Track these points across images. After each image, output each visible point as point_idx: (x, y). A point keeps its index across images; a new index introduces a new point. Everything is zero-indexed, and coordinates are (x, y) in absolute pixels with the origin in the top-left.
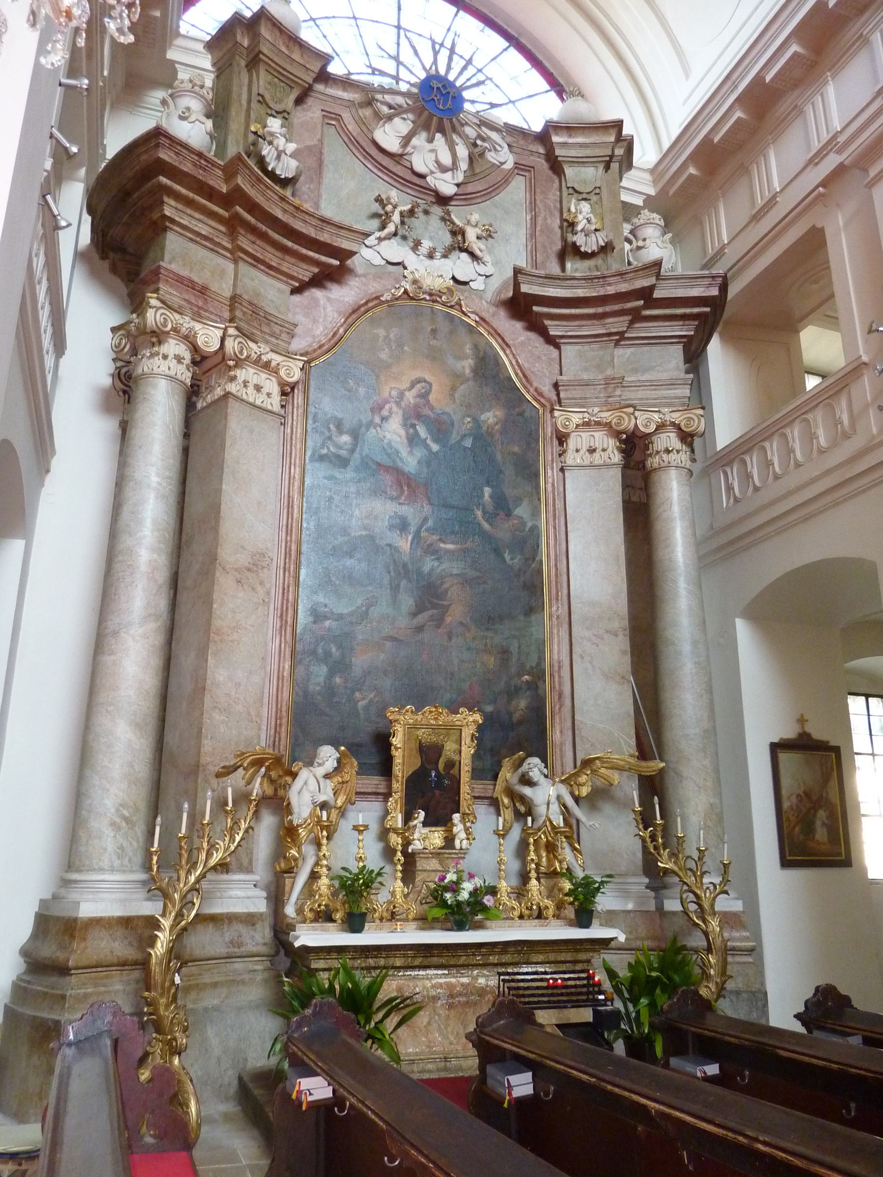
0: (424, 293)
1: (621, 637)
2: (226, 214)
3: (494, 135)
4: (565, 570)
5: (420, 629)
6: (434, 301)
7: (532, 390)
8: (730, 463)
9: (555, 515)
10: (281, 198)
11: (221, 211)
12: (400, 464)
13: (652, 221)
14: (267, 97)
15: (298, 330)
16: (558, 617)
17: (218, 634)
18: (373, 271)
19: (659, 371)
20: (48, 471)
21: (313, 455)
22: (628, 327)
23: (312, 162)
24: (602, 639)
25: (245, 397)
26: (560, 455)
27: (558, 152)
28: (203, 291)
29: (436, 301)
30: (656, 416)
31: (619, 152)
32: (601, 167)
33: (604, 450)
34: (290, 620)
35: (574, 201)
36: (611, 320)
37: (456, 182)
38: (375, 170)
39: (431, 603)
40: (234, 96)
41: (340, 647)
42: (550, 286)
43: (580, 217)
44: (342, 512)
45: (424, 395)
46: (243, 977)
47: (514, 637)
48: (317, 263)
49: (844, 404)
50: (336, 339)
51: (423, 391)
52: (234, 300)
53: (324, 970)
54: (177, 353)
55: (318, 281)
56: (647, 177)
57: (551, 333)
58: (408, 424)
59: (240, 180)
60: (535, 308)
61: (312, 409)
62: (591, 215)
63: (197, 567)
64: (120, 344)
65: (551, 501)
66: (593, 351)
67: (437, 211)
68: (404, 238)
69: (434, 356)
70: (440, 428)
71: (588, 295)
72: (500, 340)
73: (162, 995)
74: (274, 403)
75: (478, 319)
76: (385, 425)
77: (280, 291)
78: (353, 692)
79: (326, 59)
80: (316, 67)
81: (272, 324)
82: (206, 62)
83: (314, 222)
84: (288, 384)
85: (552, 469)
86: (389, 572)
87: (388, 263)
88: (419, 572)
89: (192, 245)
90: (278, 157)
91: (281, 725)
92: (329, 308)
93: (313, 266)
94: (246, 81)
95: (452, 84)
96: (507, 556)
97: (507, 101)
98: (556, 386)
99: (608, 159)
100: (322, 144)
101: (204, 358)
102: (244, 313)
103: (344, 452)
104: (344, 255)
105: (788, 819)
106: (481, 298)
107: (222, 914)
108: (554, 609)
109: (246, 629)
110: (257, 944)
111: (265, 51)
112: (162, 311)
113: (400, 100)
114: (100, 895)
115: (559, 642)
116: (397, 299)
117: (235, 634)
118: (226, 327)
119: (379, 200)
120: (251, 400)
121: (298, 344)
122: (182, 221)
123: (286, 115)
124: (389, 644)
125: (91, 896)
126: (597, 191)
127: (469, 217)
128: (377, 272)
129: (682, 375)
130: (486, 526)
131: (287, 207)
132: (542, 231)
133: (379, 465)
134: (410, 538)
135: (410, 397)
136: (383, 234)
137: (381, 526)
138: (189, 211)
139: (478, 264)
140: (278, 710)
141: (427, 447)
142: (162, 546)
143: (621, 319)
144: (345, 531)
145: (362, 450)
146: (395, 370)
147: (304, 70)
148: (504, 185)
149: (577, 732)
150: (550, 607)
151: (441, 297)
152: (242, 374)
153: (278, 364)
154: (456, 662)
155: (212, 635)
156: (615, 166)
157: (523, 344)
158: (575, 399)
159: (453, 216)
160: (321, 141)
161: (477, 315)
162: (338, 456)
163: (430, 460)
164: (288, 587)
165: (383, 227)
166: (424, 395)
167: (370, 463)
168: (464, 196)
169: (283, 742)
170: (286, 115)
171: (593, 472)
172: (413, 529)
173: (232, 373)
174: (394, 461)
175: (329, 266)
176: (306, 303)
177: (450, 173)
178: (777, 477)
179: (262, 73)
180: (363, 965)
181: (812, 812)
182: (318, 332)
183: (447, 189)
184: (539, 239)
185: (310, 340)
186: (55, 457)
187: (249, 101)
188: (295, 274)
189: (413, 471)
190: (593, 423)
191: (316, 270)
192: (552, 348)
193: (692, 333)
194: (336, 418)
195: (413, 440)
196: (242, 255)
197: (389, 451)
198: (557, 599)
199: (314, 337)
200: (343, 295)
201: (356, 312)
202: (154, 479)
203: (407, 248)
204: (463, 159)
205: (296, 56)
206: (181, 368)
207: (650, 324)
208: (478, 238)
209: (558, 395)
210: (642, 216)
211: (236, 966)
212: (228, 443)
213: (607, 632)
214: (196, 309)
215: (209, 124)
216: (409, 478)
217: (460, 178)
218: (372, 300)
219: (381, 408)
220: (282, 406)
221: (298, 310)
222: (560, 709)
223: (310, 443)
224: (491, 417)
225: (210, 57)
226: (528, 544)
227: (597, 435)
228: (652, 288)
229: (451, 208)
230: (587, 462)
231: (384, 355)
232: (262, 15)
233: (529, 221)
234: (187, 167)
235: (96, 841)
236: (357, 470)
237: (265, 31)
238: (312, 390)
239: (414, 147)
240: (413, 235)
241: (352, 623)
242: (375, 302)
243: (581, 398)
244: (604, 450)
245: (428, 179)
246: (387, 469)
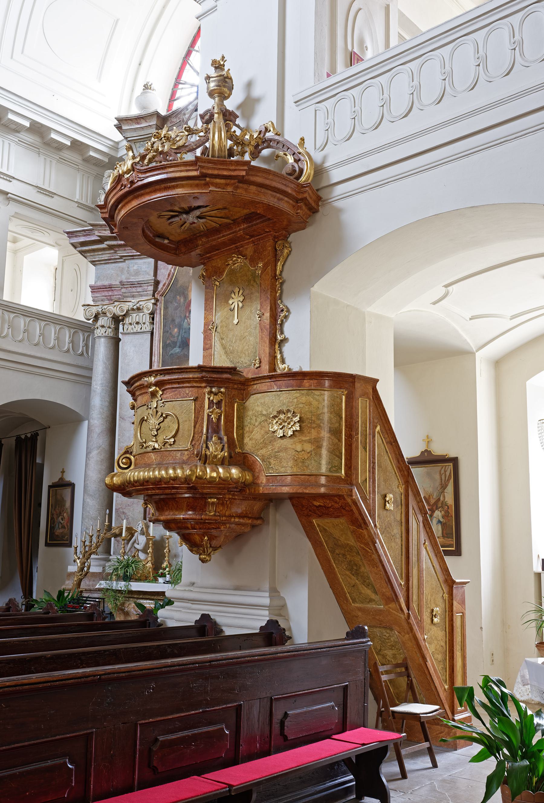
122: (96, 259)
236: (179, 347)
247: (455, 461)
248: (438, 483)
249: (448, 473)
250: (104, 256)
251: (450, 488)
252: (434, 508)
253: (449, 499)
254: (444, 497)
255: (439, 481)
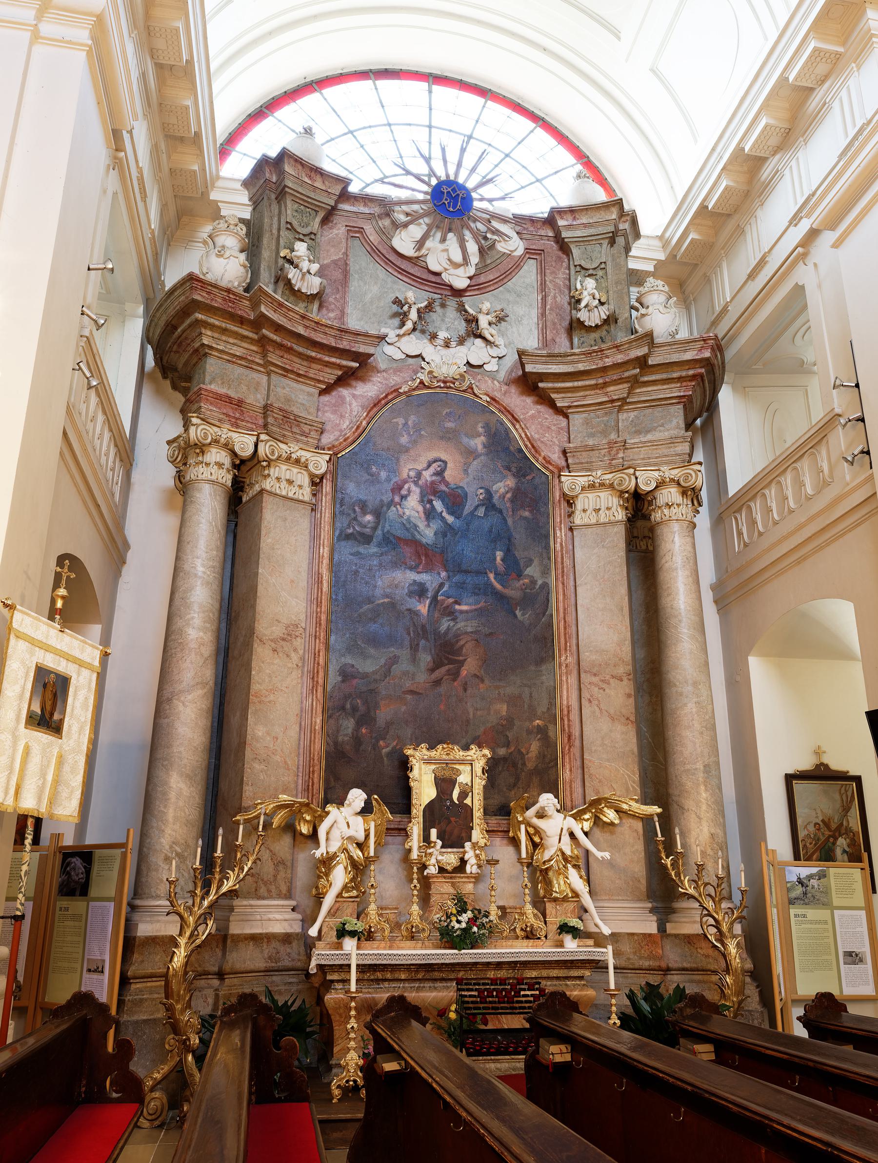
0: (438, 382)
1: (625, 682)
2: (255, 337)
3: (504, 228)
4: (574, 622)
5: (437, 683)
6: (448, 388)
7: (540, 459)
8: (739, 510)
9: (563, 572)
10: (301, 316)
11: (251, 335)
12: (418, 537)
13: (655, 288)
14: (295, 223)
15: (328, 427)
16: (567, 666)
17: (256, 697)
18: (395, 365)
19: (660, 431)
20: (124, 563)
21: (340, 535)
22: (629, 393)
23: (337, 274)
24: (609, 684)
25: (278, 492)
26: (569, 516)
27: (564, 234)
28: (239, 403)
29: (450, 387)
30: (656, 474)
31: (621, 226)
32: (605, 243)
33: (608, 509)
34: (321, 681)
35: (579, 278)
36: (612, 388)
37: (468, 275)
38: (396, 274)
39: (447, 658)
40: (266, 227)
41: (366, 702)
42: (552, 363)
43: (585, 293)
44: (367, 583)
45: (440, 473)
46: (280, 988)
47: (526, 685)
48: (340, 367)
49: (824, 453)
50: (359, 431)
51: (439, 469)
52: (266, 408)
53: (338, 981)
54: (218, 460)
55: (346, 378)
56: (658, 243)
57: (558, 405)
58: (424, 499)
59: (263, 309)
60: (541, 385)
61: (340, 495)
62: (595, 291)
63: (241, 639)
64: (173, 454)
65: (559, 560)
66: (600, 418)
67: (452, 303)
68: (423, 332)
69: (449, 437)
70: (456, 501)
71: (588, 368)
72: (510, 417)
73: (178, 1002)
74: (306, 494)
75: (488, 399)
76: (404, 502)
77: (310, 394)
78: (378, 741)
79: (346, 182)
80: (337, 190)
81: (302, 425)
82: (244, 197)
83: (333, 332)
84: (317, 476)
85: (561, 529)
86: (409, 634)
87: (407, 356)
88: (436, 633)
89: (230, 366)
90: (303, 278)
91: (313, 772)
92: (354, 404)
93: (337, 369)
94: (276, 212)
95: (462, 187)
96: (518, 613)
97: (534, 180)
98: (564, 452)
99: (611, 235)
100: (347, 256)
101: (243, 462)
102: (276, 419)
103: (368, 530)
104: (363, 359)
105: (805, 846)
106: (493, 379)
107: (261, 934)
108: (563, 658)
109: (282, 690)
110: (293, 960)
111: (290, 185)
112: (203, 427)
113: (416, 207)
114: (156, 918)
115: (568, 689)
116: (414, 390)
117: (272, 696)
118: (259, 434)
119: (397, 302)
120: (284, 493)
121: (326, 439)
122: (219, 347)
123: (313, 236)
124: (409, 697)
125: (148, 919)
126: (603, 266)
127: (480, 306)
128: (398, 366)
129: (682, 432)
130: (498, 586)
131: (307, 323)
132: (551, 309)
133: (399, 539)
134: (428, 602)
135: (427, 475)
136: (402, 332)
137: (401, 593)
138: (224, 338)
139: (491, 347)
140: (311, 759)
141: (443, 519)
142: (208, 625)
143: (621, 386)
144: (370, 600)
145: (383, 527)
146: (412, 453)
147: (326, 194)
148: (517, 271)
149: (586, 770)
150: (560, 657)
151: (454, 384)
152: (274, 472)
153: (307, 460)
154: (471, 711)
155: (251, 697)
156: (620, 241)
157: (533, 417)
158: (582, 463)
159: (467, 307)
160: (346, 254)
161: (488, 395)
162: (362, 534)
163: (447, 531)
164: (319, 652)
165: (403, 324)
166: (440, 473)
167: (391, 538)
168: (477, 286)
169: (316, 786)
170: (313, 236)
171: (599, 530)
172: (430, 595)
173: (266, 472)
174: (413, 535)
175: (355, 367)
176: (333, 401)
177: (462, 268)
178: (776, 523)
179: (289, 203)
180: (372, 977)
181: (831, 840)
182: (345, 426)
183: (461, 283)
184: (549, 317)
185: (337, 433)
186: (130, 551)
187: (279, 230)
188: (322, 379)
189: (430, 542)
190: (597, 485)
191: (340, 373)
192: (561, 418)
193: (690, 393)
194: (360, 500)
195: (430, 514)
196: (272, 368)
197: (408, 526)
198: (566, 649)
199: (341, 431)
200: (367, 390)
201: (377, 404)
202: (200, 569)
203: (426, 341)
204: (474, 254)
205: (318, 184)
206: (223, 472)
207: (650, 389)
208: (490, 324)
209: (567, 460)
210: (647, 284)
211: (274, 978)
212: (263, 533)
213: (613, 677)
214: (234, 420)
215: (243, 257)
216: (426, 548)
217: (471, 271)
218: (392, 393)
219: (400, 488)
220: (314, 495)
221: (326, 408)
222: (569, 750)
223: (338, 525)
224: (503, 486)
225: (247, 192)
226: (538, 599)
227: (602, 495)
228: (645, 358)
229: (464, 299)
230: (594, 521)
231: (404, 440)
232: (284, 154)
233: (540, 301)
234: (218, 303)
235: (154, 873)
236: (379, 545)
237: (288, 168)
238: (339, 477)
239: (429, 249)
240: (431, 329)
241: (375, 681)
242: (395, 394)
243: (587, 463)
244: (608, 509)
245: (443, 275)
246: (407, 542)
247: (858, 780)
248: (838, 805)
249: (849, 794)
250: (235, 348)
251: (855, 811)
252: (837, 834)
253: (854, 822)
254: (848, 822)
255: (839, 802)
